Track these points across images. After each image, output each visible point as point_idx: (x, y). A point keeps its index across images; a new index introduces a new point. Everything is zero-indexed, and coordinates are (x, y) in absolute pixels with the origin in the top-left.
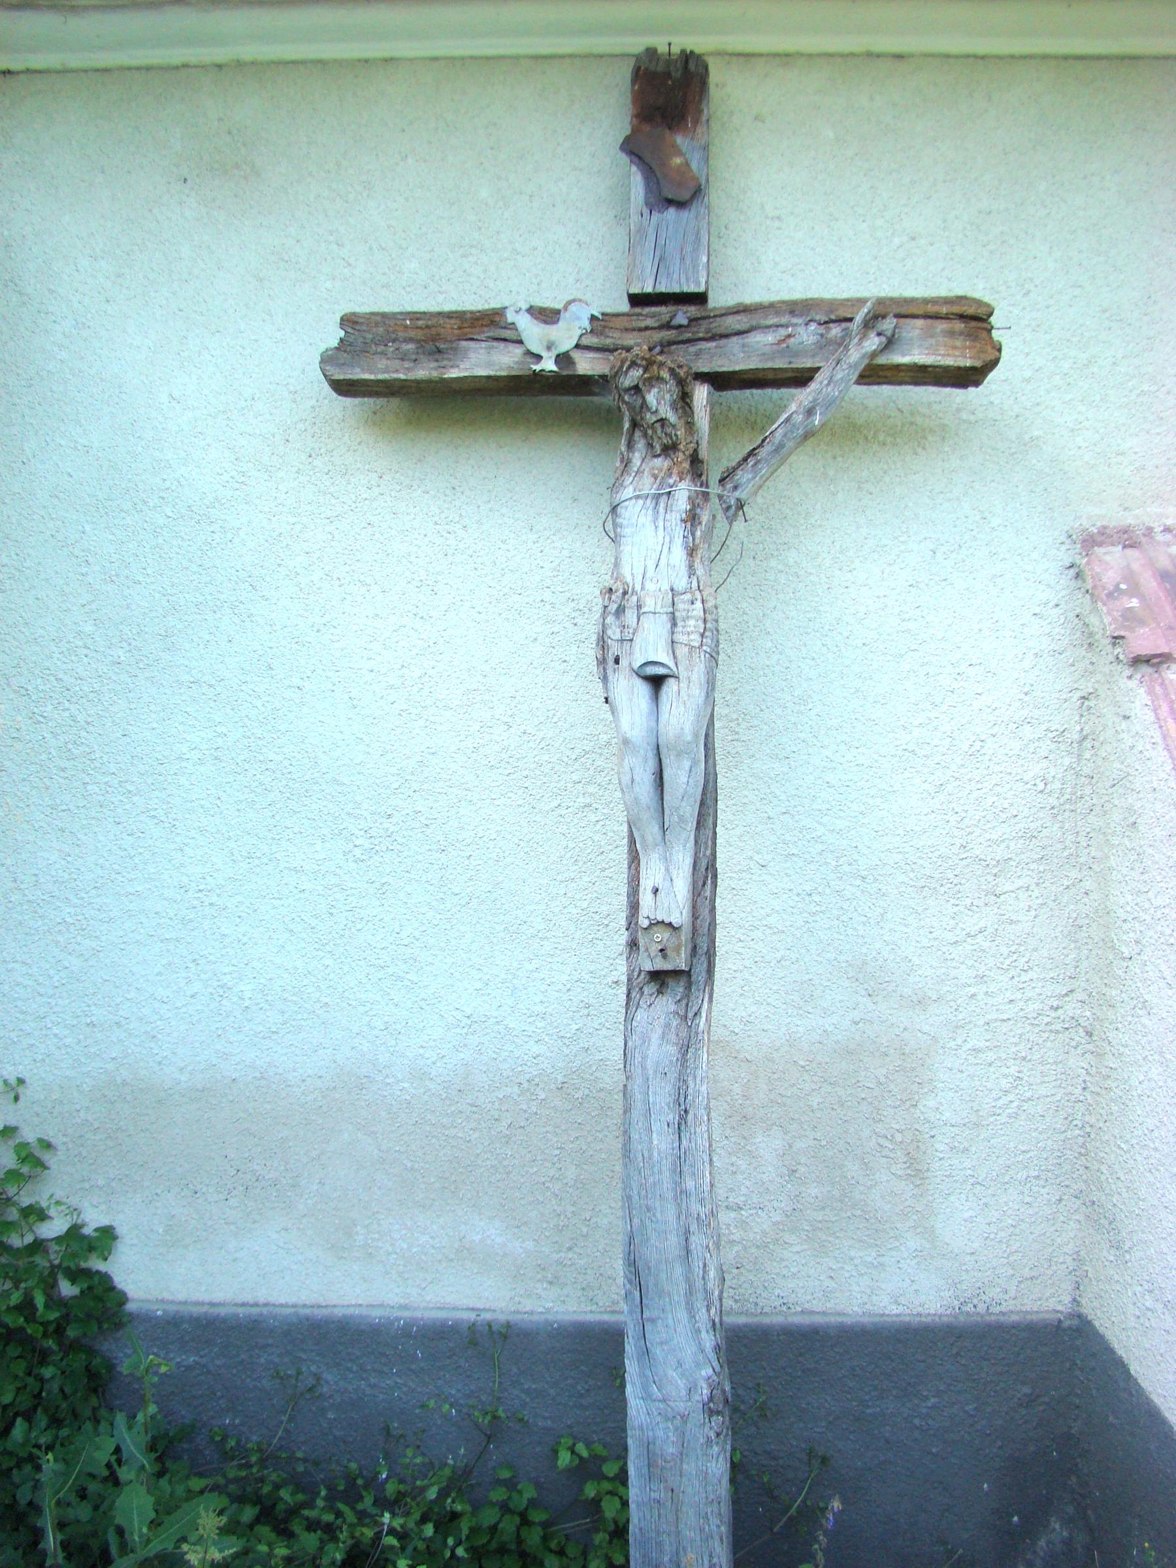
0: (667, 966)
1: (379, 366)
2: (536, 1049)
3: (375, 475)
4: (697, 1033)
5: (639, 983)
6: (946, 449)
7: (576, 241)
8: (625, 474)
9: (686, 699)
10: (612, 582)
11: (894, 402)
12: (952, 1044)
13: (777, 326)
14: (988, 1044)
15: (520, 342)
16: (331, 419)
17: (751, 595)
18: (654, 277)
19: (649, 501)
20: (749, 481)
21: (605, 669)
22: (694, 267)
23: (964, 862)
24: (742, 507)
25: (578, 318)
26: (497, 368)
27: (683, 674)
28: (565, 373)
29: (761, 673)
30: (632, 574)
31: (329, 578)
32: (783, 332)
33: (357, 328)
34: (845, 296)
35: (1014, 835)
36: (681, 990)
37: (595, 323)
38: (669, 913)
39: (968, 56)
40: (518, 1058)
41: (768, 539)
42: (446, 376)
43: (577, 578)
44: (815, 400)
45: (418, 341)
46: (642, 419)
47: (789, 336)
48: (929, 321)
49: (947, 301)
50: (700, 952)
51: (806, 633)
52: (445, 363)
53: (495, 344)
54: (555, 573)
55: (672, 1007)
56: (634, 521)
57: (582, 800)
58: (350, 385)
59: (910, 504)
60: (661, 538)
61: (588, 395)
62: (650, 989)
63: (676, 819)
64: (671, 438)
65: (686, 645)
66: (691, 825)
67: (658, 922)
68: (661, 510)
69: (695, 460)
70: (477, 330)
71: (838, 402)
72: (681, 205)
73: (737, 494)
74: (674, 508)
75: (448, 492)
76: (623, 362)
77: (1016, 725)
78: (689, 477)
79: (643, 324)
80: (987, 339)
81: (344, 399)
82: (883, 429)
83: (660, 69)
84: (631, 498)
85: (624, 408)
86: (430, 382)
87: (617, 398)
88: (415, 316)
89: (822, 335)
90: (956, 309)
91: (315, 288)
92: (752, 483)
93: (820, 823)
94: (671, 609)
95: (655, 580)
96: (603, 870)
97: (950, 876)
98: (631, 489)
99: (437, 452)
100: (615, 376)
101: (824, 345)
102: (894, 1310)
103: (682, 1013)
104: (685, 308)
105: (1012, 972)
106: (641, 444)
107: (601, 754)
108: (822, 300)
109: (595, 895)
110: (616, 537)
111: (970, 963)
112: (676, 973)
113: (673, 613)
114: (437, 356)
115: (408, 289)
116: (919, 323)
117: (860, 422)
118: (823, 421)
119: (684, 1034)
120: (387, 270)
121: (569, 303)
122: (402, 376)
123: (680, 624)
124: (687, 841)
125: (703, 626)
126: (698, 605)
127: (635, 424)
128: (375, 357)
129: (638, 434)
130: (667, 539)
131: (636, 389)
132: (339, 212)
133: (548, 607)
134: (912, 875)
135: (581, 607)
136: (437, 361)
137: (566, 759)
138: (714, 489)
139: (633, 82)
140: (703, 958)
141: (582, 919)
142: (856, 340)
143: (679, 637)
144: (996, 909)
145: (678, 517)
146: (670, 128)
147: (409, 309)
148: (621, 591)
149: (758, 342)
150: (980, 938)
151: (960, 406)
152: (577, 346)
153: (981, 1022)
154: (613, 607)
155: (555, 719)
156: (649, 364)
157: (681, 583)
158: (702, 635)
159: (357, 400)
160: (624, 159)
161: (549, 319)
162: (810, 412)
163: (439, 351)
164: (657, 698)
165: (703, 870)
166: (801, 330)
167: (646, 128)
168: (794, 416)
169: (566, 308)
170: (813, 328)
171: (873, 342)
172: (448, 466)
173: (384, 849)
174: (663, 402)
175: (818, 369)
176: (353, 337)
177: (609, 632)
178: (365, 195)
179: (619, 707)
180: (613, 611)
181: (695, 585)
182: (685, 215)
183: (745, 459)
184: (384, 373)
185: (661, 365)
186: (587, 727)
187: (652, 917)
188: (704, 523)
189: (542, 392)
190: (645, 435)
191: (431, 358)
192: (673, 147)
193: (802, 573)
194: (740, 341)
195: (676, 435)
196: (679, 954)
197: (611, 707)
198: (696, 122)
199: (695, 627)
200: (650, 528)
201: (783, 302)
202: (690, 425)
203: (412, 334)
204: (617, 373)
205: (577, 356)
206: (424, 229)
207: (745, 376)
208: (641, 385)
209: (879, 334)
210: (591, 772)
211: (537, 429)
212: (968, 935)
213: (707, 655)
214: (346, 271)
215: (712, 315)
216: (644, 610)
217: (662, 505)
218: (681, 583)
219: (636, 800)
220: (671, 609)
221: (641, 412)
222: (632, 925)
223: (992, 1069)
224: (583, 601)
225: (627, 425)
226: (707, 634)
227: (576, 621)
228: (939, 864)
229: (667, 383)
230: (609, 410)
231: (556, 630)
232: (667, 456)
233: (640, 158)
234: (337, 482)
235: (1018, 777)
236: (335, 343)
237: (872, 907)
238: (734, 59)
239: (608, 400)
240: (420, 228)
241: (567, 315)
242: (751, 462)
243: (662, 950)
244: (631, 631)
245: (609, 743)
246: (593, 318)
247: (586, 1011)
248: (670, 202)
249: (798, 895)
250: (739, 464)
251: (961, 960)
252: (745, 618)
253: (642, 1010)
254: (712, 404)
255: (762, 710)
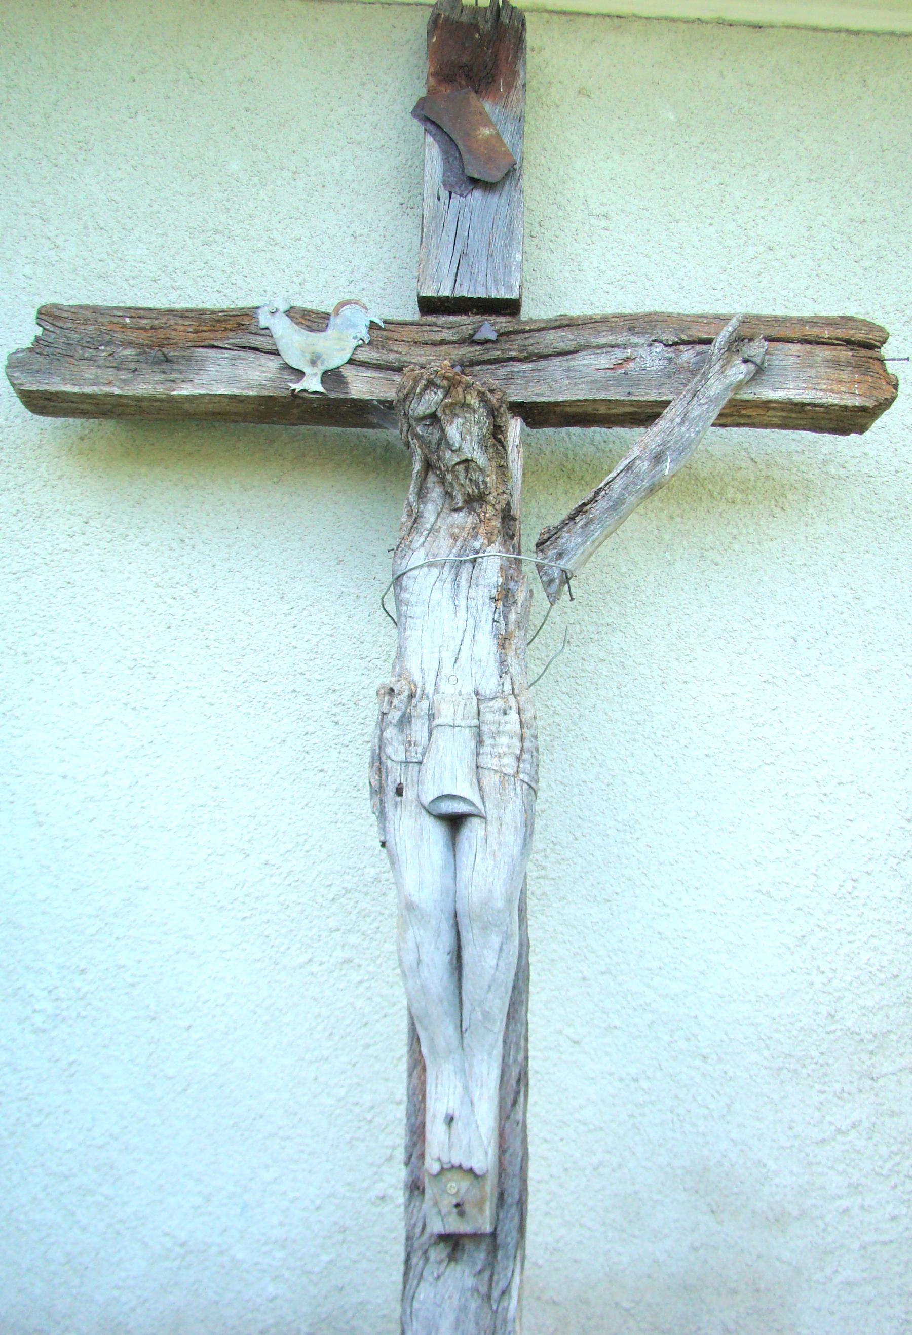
0: (464, 1227)
1: (87, 376)
2: (271, 1290)
3: (78, 520)
4: (505, 1321)
5: (422, 1245)
6: (810, 511)
7: (350, 232)
8: (414, 532)
9: (496, 848)
10: (394, 679)
11: (746, 450)
13: (612, 346)
14: (865, 1274)
15: (276, 353)
16: (24, 443)
17: (564, 690)
18: (453, 277)
19: (447, 568)
20: (577, 546)
21: (381, 801)
22: (505, 267)
23: (832, 1036)
24: (567, 580)
25: (354, 326)
26: (244, 385)
27: (491, 812)
28: (333, 396)
29: (576, 790)
30: (422, 670)
31: (12, 652)
32: (620, 354)
33: (59, 324)
34: (697, 310)
35: (894, 1000)
36: (482, 1255)
37: (376, 333)
38: (470, 1154)
39: (839, 31)
40: (248, 1301)
41: (586, 618)
42: (175, 393)
43: (340, 663)
44: (664, 443)
45: (140, 346)
46: (439, 459)
47: (628, 359)
48: (808, 347)
49: (830, 322)
50: (509, 1200)
51: (634, 740)
52: (175, 375)
53: (242, 354)
54: (312, 656)
55: (470, 1282)
56: (426, 597)
57: (340, 954)
58: (46, 399)
59: (765, 579)
60: (462, 624)
61: (362, 427)
62: (438, 1253)
63: (479, 1016)
64: (477, 486)
65: (496, 771)
66: (499, 1026)
67: (453, 1167)
68: (464, 583)
69: (507, 517)
70: (219, 335)
71: (693, 447)
72: (489, 187)
73: (562, 563)
74: (481, 581)
75: (174, 545)
76: (416, 381)
77: (897, 861)
78: (499, 540)
79: (437, 337)
80: (881, 371)
81: (42, 418)
82: (732, 483)
83: (464, 19)
84: (421, 566)
85: (414, 443)
86: (153, 399)
87: (405, 429)
88: (137, 313)
89: (670, 359)
90: (840, 333)
91: (10, 273)
92: (582, 548)
93: (649, 986)
94: (476, 722)
95: (453, 679)
96: (367, 1046)
97: (815, 1054)
98: (421, 553)
99: (162, 493)
100: (404, 400)
101: (673, 371)
103: (483, 1289)
104: (493, 318)
105: (894, 1179)
106: (436, 493)
107: (366, 894)
108: (670, 315)
109: (355, 1080)
110: (399, 616)
111: (840, 1167)
112: (476, 1237)
113: (479, 727)
114: (165, 366)
115: (132, 282)
116: (795, 348)
117: (704, 473)
118: (674, 471)
119: (487, 1321)
120: (105, 257)
121: (343, 304)
122: (117, 391)
123: (488, 741)
124: (492, 1047)
125: (519, 745)
126: (513, 716)
127: (428, 466)
128: (81, 362)
129: (432, 478)
130: (471, 623)
131: (433, 418)
132: (45, 178)
133: (302, 699)
134: (766, 1053)
135: (344, 701)
136: (164, 372)
137: (319, 900)
138: (530, 558)
139: (430, 33)
140: (514, 1210)
141: (338, 1111)
142: (717, 367)
143: (486, 761)
144: (873, 1097)
145: (487, 594)
146: (476, 92)
147: (129, 304)
148: (406, 693)
149: (587, 366)
150: (852, 1135)
151: (828, 457)
152: (351, 362)
153: (856, 1246)
154: (395, 716)
155: (307, 847)
156: (452, 385)
157: (489, 685)
158: (518, 759)
159: (59, 421)
160: (417, 127)
161: (314, 326)
162: (658, 459)
163: (168, 360)
164: (455, 850)
165: (513, 1082)
166: (643, 352)
167: (446, 90)
168: (638, 462)
169: (337, 311)
170: (658, 350)
171: (739, 371)
172: (176, 512)
173: (74, 1015)
174: (468, 437)
175: (668, 403)
176: (53, 335)
177: (389, 750)
178: (80, 158)
179: (402, 858)
180: (395, 721)
181: (508, 687)
182: (492, 200)
183: (572, 518)
184: (95, 384)
185: (468, 387)
186: (349, 858)
187: (445, 1159)
188: (520, 602)
189: (302, 421)
190: (442, 481)
191: (155, 368)
192: (481, 114)
193: (629, 663)
194: (564, 363)
195: (484, 482)
196: (481, 1210)
197: (390, 853)
198: (510, 86)
199: (509, 747)
200: (448, 605)
201: (620, 316)
202: (503, 470)
203: (132, 336)
204: (407, 396)
205: (350, 373)
206: (156, 207)
207: (568, 409)
208: (439, 414)
209: (745, 361)
210: (353, 917)
211: (294, 469)
212: (839, 1131)
213: (525, 786)
214: (52, 253)
215: (528, 328)
216: (437, 721)
217: (464, 576)
218: (489, 685)
219: (424, 989)
220: (476, 722)
221: (438, 448)
222: (413, 1159)
223: (871, 1309)
224: (347, 694)
225: (417, 467)
226: (526, 756)
227: (338, 718)
228: (800, 1038)
229: (474, 411)
230: (388, 448)
231: (311, 729)
232: (471, 510)
233: (438, 126)
234: (28, 527)
235: (900, 926)
236: (28, 343)
237: (716, 1095)
238: (555, 17)
239: (392, 434)
240: (150, 205)
241: (339, 320)
242: (581, 521)
243: (457, 1205)
244: (420, 749)
245: (377, 880)
246: (373, 326)
247: (340, 1237)
248: (475, 183)
249: (621, 1080)
250: (564, 524)
251: (830, 1164)
252: (557, 719)
253: (427, 1285)
254: (525, 442)
255: (576, 839)
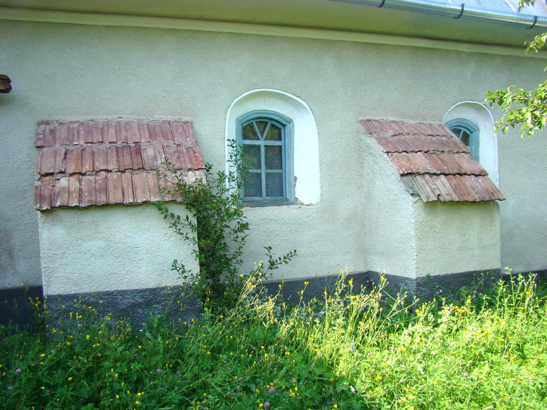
12: (17, 229)
102: (9, 286)
105: (29, 213)
150: (21, 207)
